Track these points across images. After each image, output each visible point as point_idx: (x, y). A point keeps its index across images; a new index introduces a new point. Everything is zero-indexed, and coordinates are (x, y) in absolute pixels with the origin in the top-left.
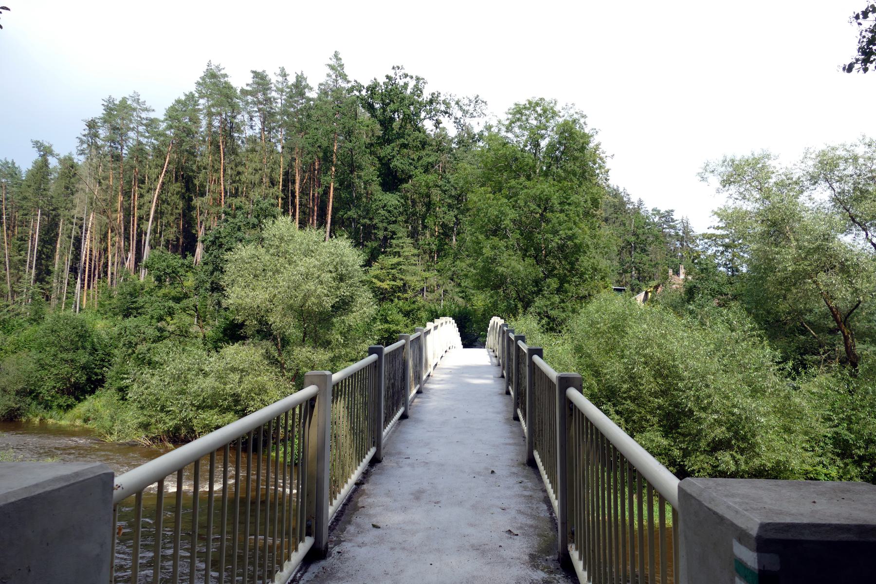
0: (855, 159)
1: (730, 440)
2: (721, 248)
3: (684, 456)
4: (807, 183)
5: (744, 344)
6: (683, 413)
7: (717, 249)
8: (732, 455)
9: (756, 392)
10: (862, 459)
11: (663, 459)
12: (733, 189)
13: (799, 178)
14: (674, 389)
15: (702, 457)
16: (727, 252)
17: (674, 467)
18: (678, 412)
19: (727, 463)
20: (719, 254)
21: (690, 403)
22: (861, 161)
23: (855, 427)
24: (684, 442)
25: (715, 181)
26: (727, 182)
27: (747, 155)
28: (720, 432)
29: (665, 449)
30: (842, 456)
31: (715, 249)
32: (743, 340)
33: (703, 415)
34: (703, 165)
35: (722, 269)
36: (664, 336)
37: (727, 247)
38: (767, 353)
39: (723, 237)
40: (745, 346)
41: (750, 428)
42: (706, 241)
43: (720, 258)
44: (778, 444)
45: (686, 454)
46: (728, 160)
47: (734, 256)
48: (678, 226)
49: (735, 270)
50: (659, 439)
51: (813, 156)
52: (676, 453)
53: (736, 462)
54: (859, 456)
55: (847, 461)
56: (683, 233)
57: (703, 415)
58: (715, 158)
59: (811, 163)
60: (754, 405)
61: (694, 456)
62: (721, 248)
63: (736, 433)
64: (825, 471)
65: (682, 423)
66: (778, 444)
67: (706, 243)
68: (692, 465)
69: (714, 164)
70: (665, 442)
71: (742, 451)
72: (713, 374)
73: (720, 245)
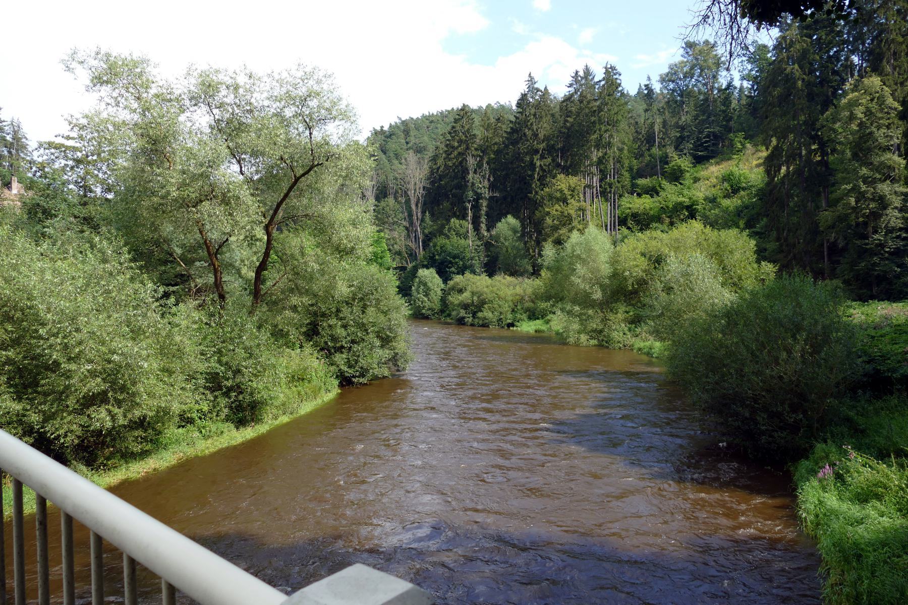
0: (236, 88)
1: (105, 393)
2: (70, 163)
3: (46, 420)
4: (187, 103)
5: (121, 278)
6: (47, 368)
7: (66, 163)
8: (109, 412)
9: (136, 334)
10: (230, 389)
11: (15, 428)
12: (106, 90)
13: (180, 95)
14: (31, 337)
15: (69, 418)
16: (78, 168)
17: (30, 436)
18: (37, 366)
19: (102, 421)
20: (68, 169)
21: (55, 353)
22: (241, 91)
23: (224, 359)
24: (45, 403)
25: (84, 76)
26: (98, 80)
27: (125, 54)
28: (96, 385)
29: (18, 415)
30: (212, 390)
31: (63, 162)
32: (119, 273)
33: (73, 367)
34: (70, 52)
35: (71, 186)
36: (15, 267)
37: (78, 162)
38: (148, 288)
39: (75, 149)
40: (121, 280)
41: (130, 375)
42: (53, 151)
43: (70, 174)
44: (160, 389)
45: (48, 418)
46: (103, 52)
47: (87, 173)
48: (6, 128)
49: (87, 189)
50: (9, 403)
51: (195, 74)
52: (34, 418)
53: (113, 417)
54: (227, 388)
55: (216, 393)
56: (13, 139)
57: (73, 367)
58: (86, 48)
59: (193, 81)
60: (136, 349)
61: (59, 419)
62: (70, 163)
63: (114, 383)
64: (197, 406)
65: (42, 379)
66: (160, 389)
67: (52, 154)
68: (57, 429)
69: (84, 54)
70: (17, 407)
71: (119, 403)
72: (86, 315)
73: (71, 159)
